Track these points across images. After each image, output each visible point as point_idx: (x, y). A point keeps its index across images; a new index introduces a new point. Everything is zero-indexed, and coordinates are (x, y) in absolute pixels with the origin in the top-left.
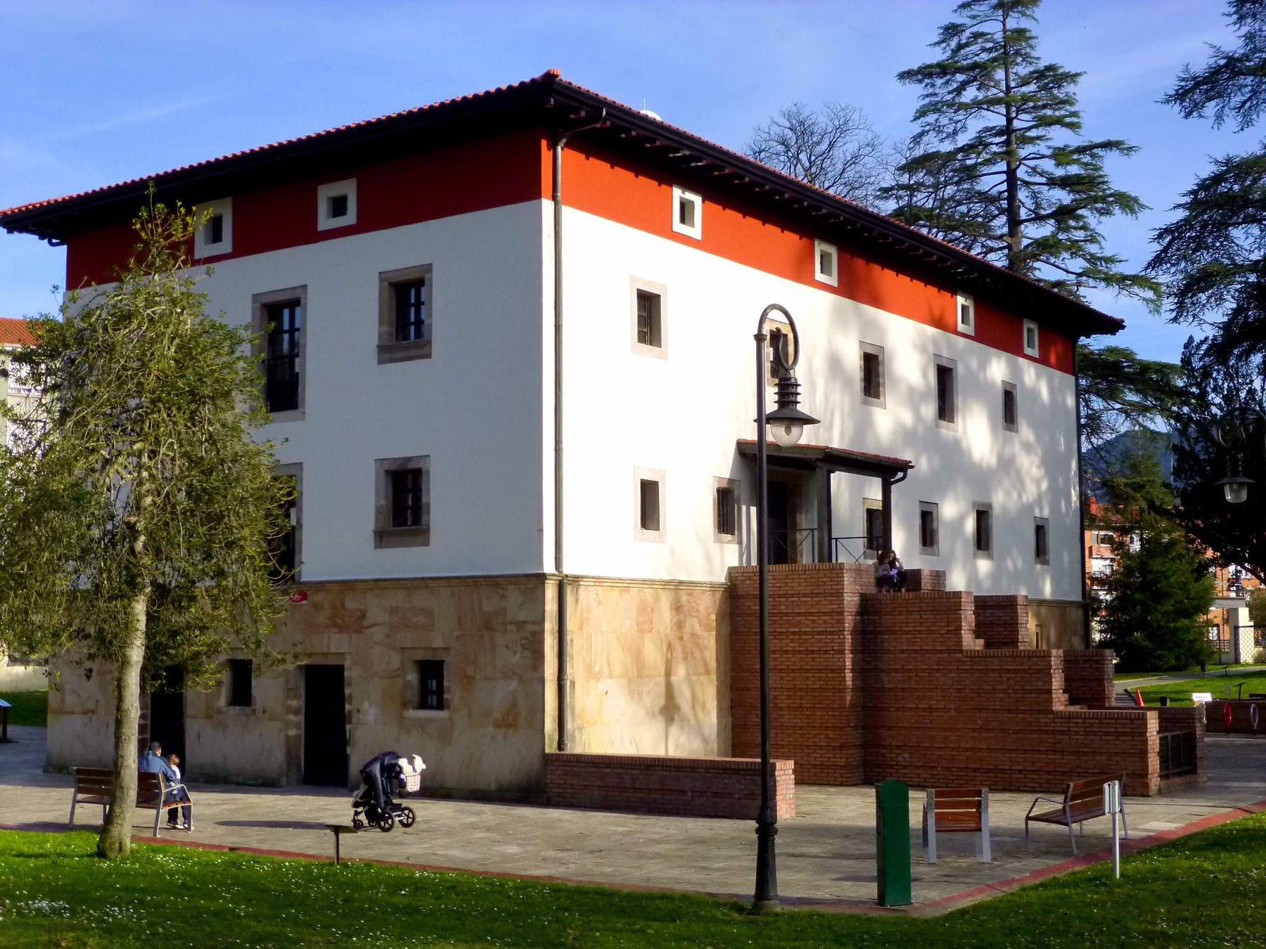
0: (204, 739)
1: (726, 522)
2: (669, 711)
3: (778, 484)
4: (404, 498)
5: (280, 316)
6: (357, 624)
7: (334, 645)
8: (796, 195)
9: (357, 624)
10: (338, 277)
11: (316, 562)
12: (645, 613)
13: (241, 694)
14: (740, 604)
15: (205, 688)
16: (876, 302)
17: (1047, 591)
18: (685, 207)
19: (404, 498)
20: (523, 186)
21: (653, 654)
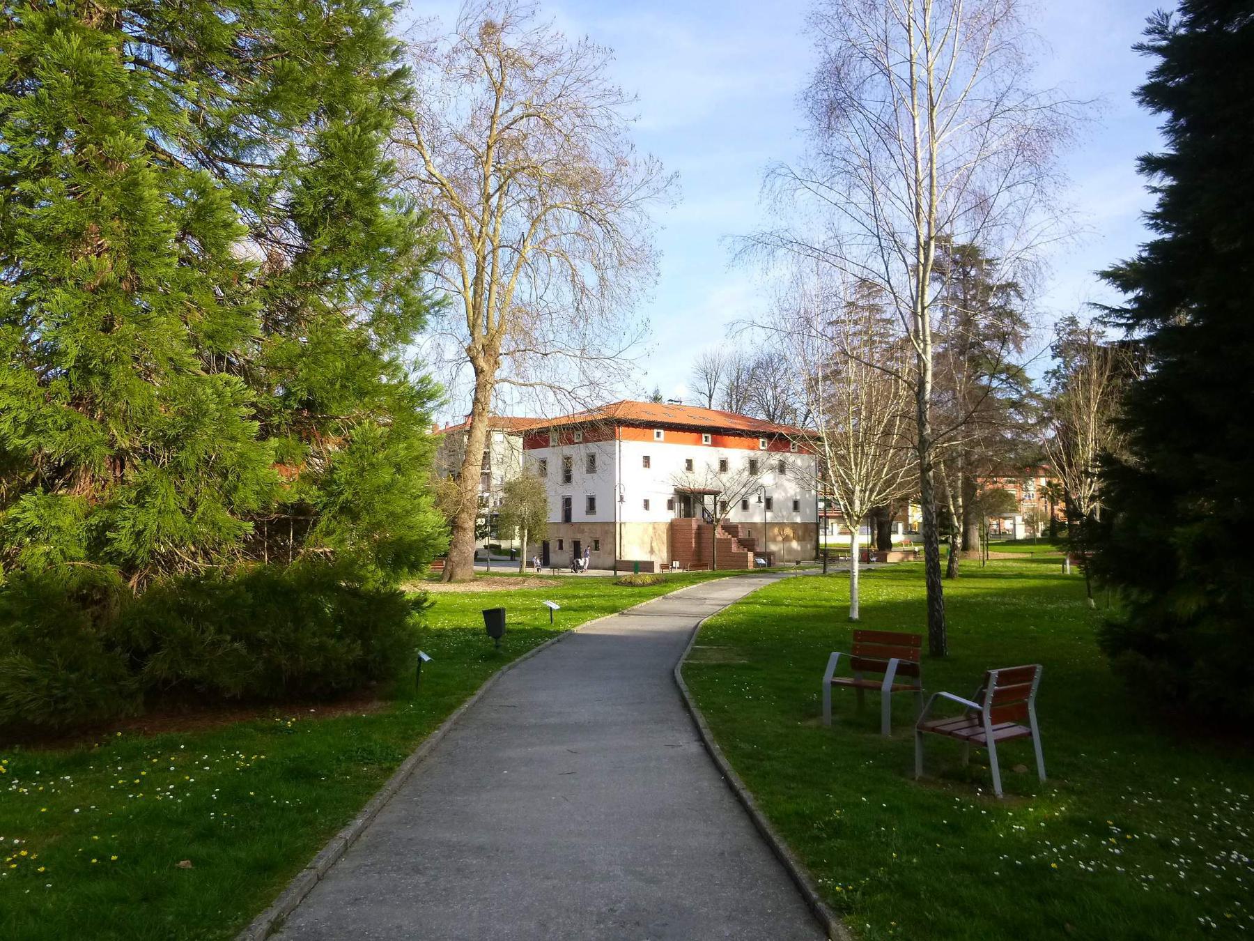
0: (553, 558)
1: (670, 505)
2: (652, 551)
3: (687, 499)
4: (591, 504)
5: (567, 461)
6: (583, 532)
7: (578, 537)
8: (566, 602)
9: (583, 532)
10: (578, 453)
11: (574, 519)
12: (646, 530)
13: (561, 548)
14: (673, 528)
15: (553, 546)
16: (724, 446)
17: (798, 520)
18: (658, 434)
19: (591, 504)
20: (613, 437)
21: (647, 540)
